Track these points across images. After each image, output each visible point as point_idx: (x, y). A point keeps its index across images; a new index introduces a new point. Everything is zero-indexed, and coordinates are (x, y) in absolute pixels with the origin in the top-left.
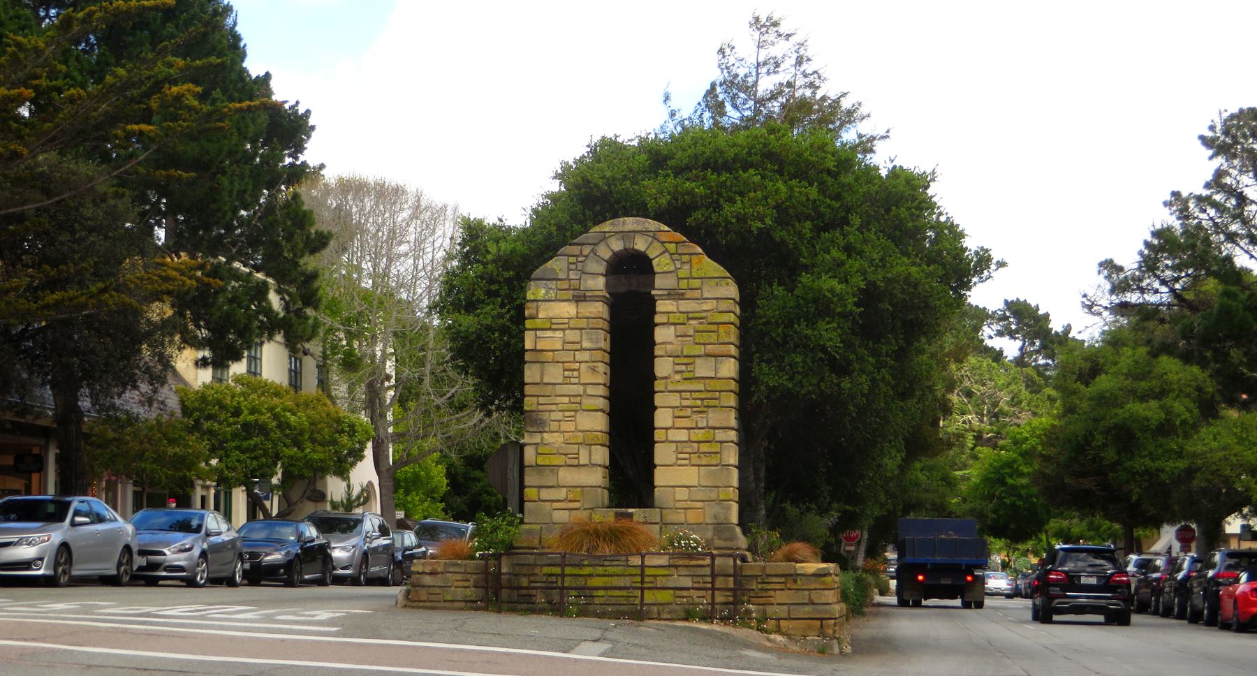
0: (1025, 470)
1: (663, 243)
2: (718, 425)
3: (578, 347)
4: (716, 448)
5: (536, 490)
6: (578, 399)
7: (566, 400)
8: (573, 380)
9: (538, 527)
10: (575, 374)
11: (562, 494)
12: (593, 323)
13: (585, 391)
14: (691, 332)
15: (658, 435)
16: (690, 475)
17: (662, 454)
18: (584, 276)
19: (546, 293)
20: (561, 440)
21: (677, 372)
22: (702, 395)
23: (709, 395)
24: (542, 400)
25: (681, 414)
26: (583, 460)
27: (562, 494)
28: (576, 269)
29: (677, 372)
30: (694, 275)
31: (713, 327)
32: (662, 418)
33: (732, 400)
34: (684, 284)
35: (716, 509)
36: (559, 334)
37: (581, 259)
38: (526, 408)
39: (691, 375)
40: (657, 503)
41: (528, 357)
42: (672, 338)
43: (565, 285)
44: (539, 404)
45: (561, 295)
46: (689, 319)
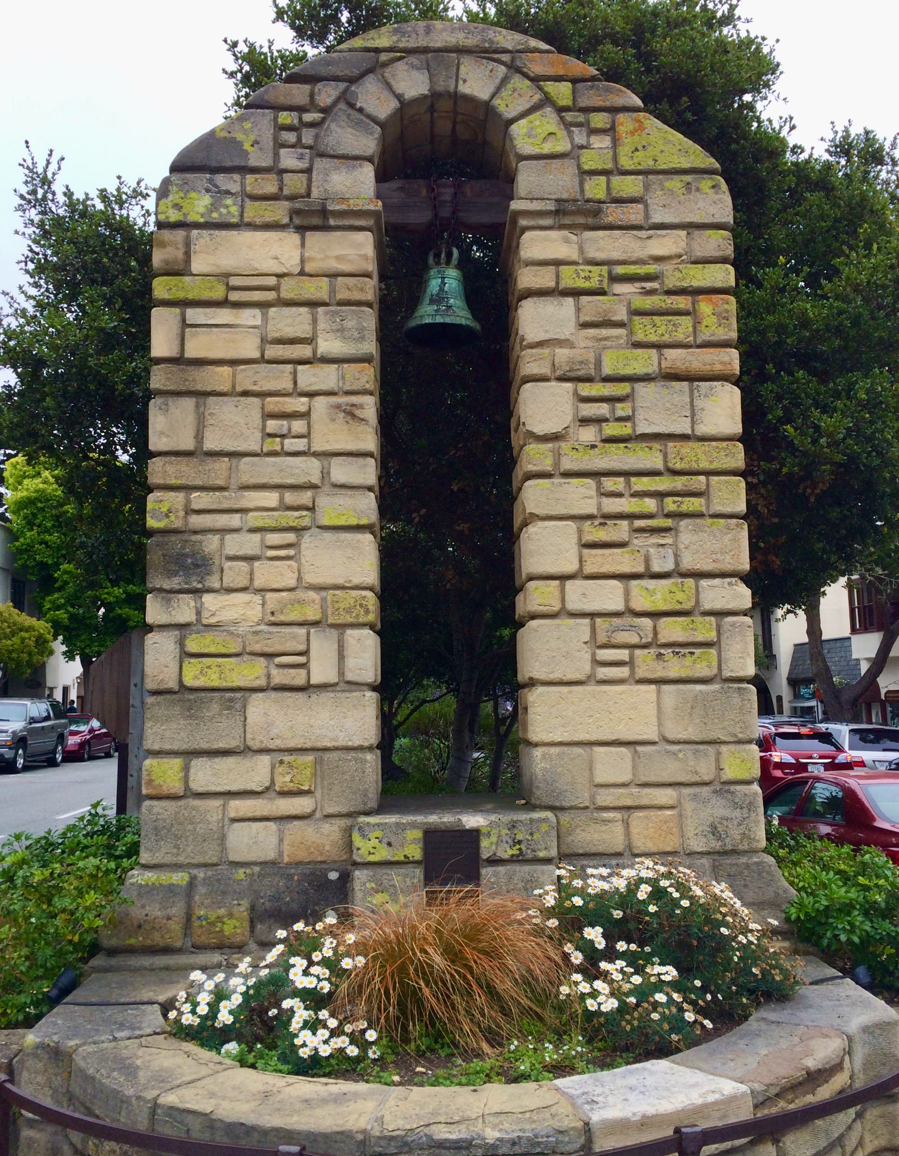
0: (21, 873)
1: (536, 80)
2: (707, 566)
3: (305, 351)
4: (705, 630)
5: (177, 763)
6: (305, 497)
7: (271, 499)
8: (291, 444)
9: (180, 878)
10: (298, 426)
11: (255, 772)
12: (346, 289)
13: (325, 474)
14: (621, 315)
15: (536, 597)
16: (634, 710)
17: (545, 649)
18: (320, 164)
19: (214, 207)
20: (255, 613)
21: (585, 421)
22: (663, 484)
23: (679, 483)
24: (200, 500)
25: (602, 535)
26: (322, 670)
27: (255, 772)
28: (298, 144)
29: (585, 421)
30: (626, 163)
31: (682, 302)
32: (545, 548)
33: (733, 496)
34: (596, 188)
35: (718, 809)
36: (250, 317)
37: (308, 117)
38: (152, 523)
39: (625, 429)
40: (540, 794)
41: (158, 379)
42: (568, 330)
43: (269, 186)
44: (190, 511)
45: (255, 211)
46: (615, 279)
